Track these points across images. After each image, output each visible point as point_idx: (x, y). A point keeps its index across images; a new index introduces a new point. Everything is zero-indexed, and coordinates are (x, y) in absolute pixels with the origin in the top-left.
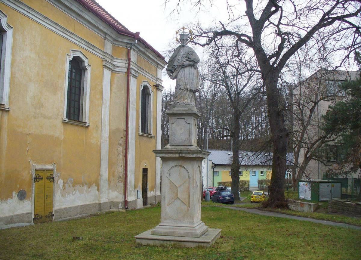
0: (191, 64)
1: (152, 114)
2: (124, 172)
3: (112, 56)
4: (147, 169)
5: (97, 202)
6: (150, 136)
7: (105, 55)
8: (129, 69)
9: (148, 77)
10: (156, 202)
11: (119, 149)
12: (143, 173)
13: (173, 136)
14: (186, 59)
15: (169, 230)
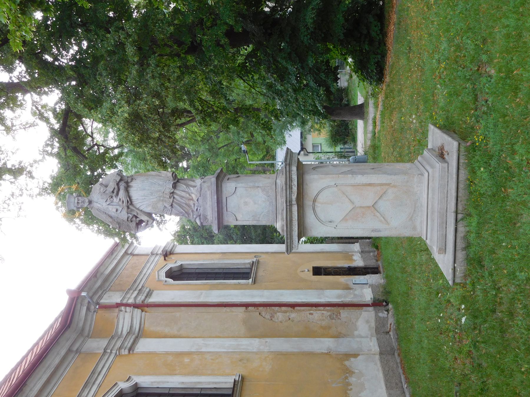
0: (125, 187)
1: (216, 262)
2: (322, 308)
3: (113, 338)
4: (313, 267)
5: (378, 357)
6: (256, 264)
7: (109, 351)
8: (136, 306)
9: (149, 271)
10: (372, 252)
11: (280, 320)
12: (321, 275)
13: (259, 218)
14: (114, 198)
15: (436, 221)
